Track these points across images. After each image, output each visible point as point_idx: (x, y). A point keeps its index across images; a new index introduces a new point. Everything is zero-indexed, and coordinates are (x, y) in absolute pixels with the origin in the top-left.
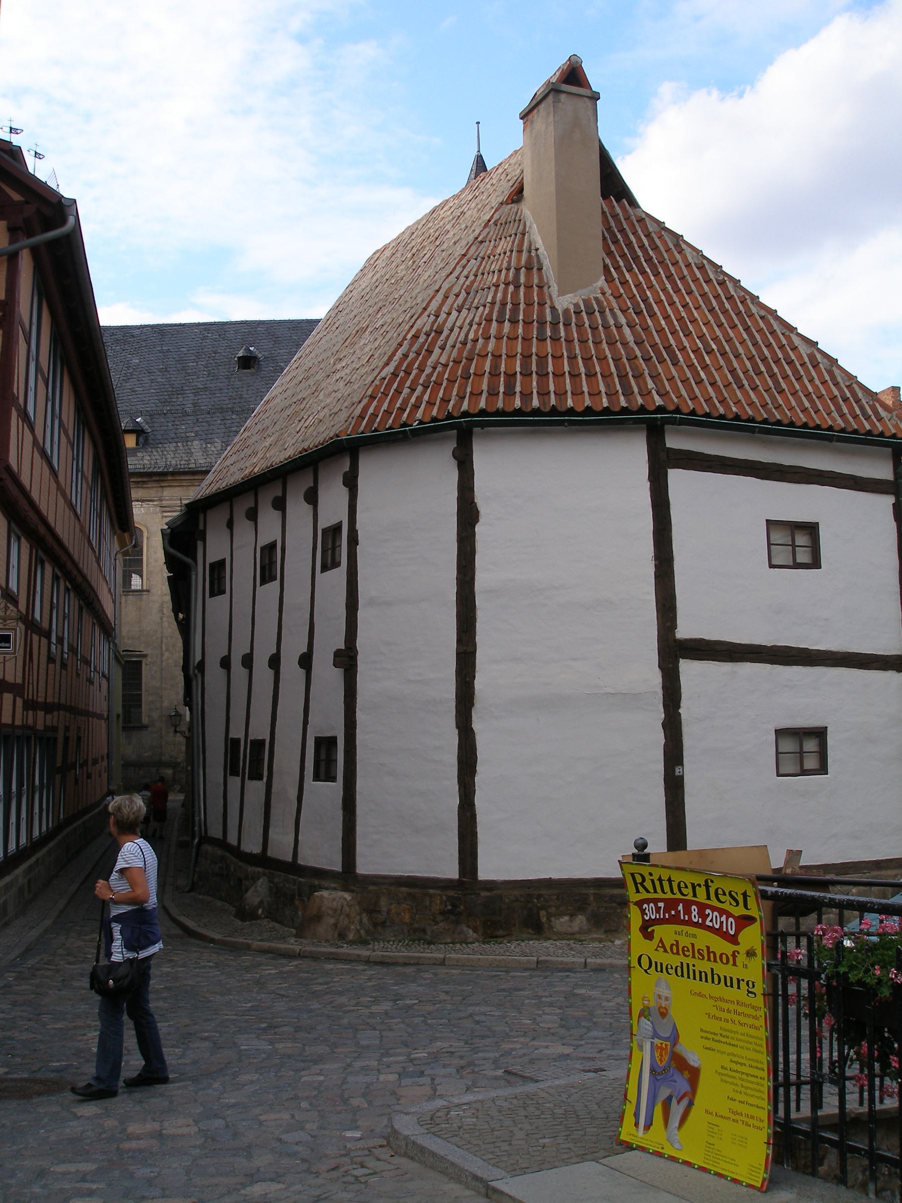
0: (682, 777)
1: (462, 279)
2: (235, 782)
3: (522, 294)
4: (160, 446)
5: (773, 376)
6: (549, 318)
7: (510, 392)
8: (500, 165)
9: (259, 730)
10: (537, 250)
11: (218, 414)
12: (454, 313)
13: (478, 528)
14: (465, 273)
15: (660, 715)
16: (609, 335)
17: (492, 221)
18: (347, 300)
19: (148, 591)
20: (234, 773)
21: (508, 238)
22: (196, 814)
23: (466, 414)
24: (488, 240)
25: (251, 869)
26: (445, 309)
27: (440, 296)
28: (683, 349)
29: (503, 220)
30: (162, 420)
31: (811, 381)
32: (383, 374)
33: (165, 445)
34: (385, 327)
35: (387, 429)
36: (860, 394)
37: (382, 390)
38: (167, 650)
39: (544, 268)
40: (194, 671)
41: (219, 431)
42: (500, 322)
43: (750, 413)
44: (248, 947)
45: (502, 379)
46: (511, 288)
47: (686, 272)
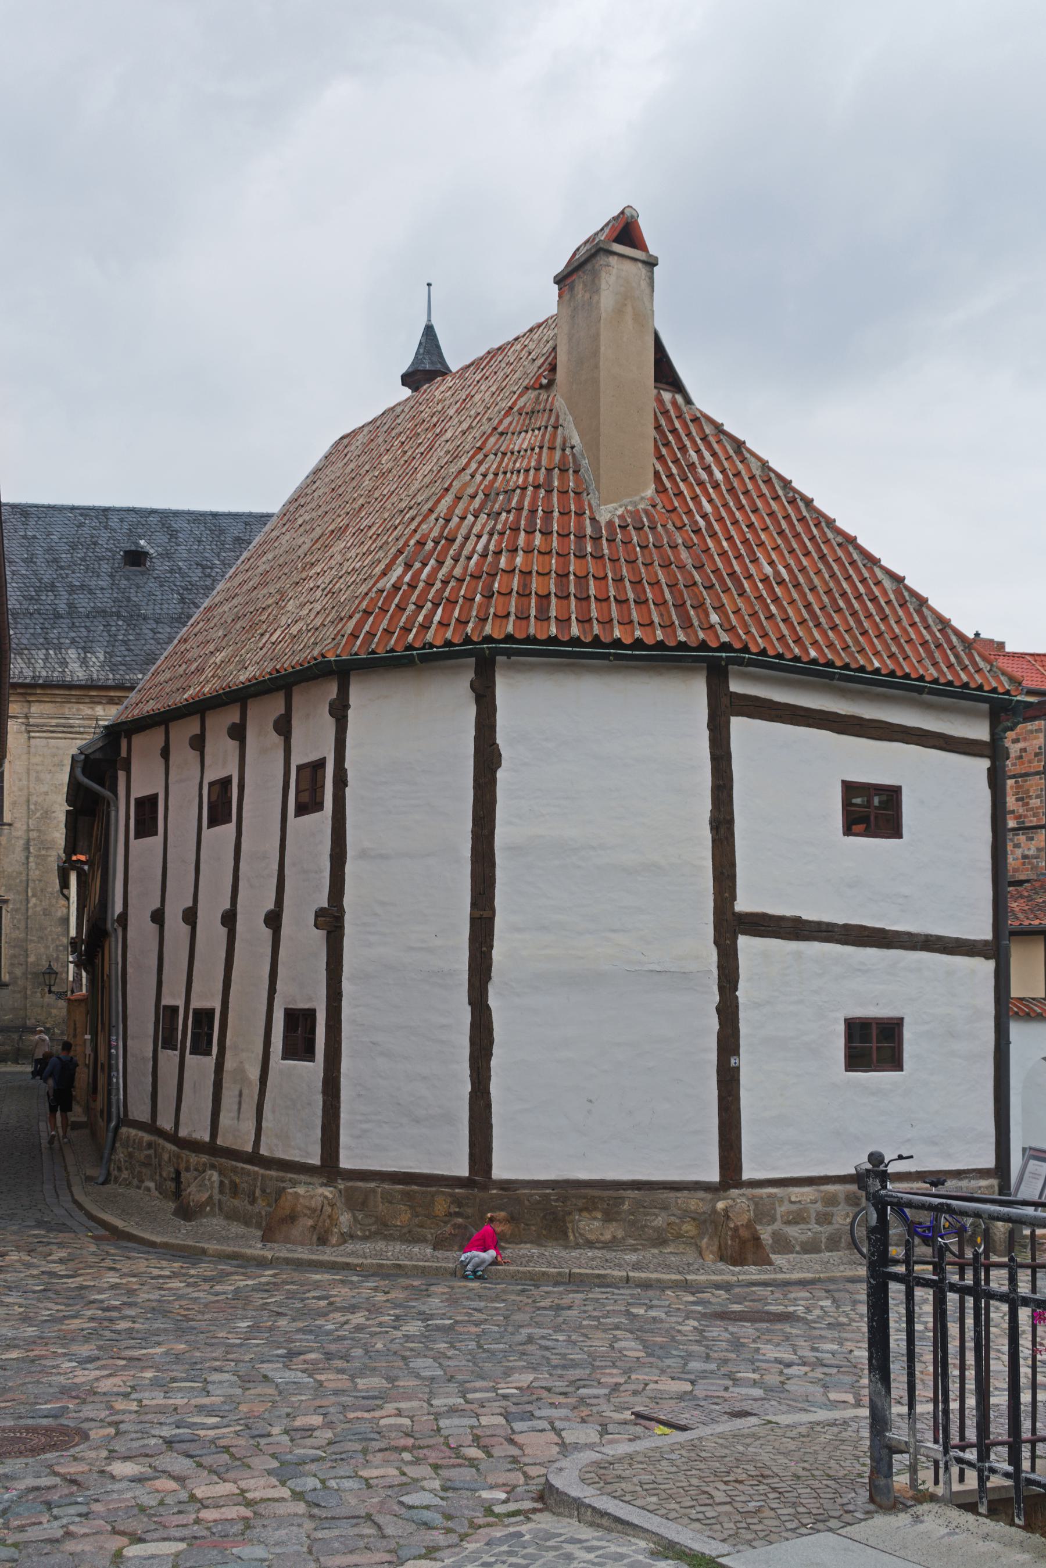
0: (738, 1068)
1: (479, 477)
2: (169, 1058)
3: (555, 499)
4: (26, 652)
5: (854, 613)
6: (589, 531)
7: (543, 617)
8: (516, 339)
9: (207, 997)
10: (572, 447)
11: (100, 619)
12: (470, 518)
13: (500, 774)
14: (482, 469)
15: (715, 997)
16: (663, 556)
17: (515, 409)
18: (310, 492)
19: (10, 825)
20: (169, 1043)
21: (536, 432)
22: (114, 1092)
23: (488, 639)
24: (511, 430)
25: (194, 1159)
26: (458, 511)
27: (449, 499)
28: (749, 577)
29: (528, 409)
30: (28, 621)
31: (898, 622)
32: (379, 585)
33: (33, 652)
34: (373, 529)
35: (387, 652)
36: (954, 639)
37: (380, 604)
38: (34, 895)
39: (582, 470)
40: (113, 924)
41: (101, 639)
42: (530, 533)
43: (830, 656)
44: (204, 1252)
45: (533, 601)
46: (542, 493)
47: (750, 487)
